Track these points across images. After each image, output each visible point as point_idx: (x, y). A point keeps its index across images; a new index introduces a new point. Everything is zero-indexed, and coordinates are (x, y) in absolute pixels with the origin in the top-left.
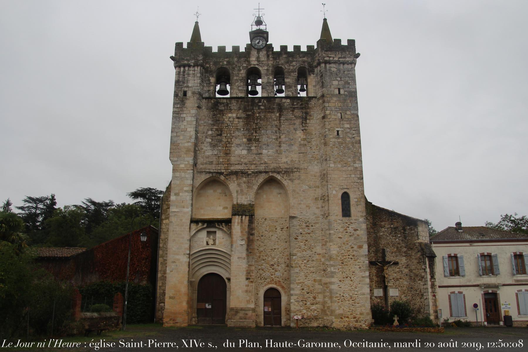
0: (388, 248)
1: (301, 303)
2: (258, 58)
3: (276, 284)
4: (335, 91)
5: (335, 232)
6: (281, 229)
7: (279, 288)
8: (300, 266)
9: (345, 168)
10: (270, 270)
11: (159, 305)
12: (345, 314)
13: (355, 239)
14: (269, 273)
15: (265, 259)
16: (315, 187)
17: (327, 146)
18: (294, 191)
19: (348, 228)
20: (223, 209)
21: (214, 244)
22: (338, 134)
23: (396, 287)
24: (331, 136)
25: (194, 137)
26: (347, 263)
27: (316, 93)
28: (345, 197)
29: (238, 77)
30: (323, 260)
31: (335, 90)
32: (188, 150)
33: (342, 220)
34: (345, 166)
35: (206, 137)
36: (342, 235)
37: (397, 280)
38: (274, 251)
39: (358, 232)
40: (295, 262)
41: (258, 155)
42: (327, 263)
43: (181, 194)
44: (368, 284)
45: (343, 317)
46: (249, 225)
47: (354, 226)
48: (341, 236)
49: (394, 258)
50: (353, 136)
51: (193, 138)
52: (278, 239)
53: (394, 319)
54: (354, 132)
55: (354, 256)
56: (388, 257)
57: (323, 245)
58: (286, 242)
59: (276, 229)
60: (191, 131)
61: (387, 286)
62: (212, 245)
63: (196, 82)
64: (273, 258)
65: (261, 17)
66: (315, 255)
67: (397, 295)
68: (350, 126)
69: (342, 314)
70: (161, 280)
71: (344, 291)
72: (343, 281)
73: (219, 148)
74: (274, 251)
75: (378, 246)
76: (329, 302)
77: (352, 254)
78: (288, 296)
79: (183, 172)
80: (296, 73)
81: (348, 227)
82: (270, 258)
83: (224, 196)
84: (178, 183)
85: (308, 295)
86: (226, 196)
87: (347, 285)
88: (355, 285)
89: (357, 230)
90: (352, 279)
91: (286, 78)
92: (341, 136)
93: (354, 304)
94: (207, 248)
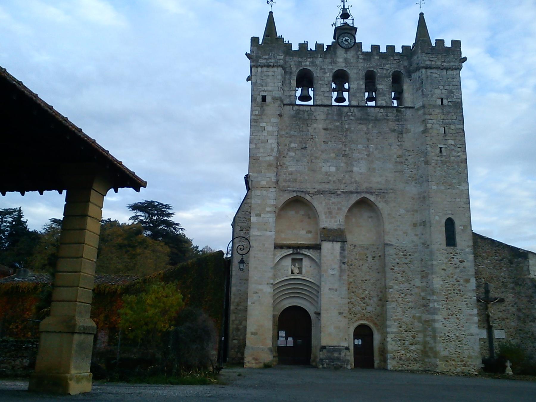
0: (492, 283)
1: (399, 343)
2: (346, 60)
3: (367, 320)
4: (437, 101)
5: (438, 263)
6: (372, 258)
7: (371, 325)
8: (396, 300)
9: (449, 190)
10: (360, 304)
11: (232, 341)
12: (450, 357)
13: (461, 271)
14: (359, 307)
15: (355, 291)
16: (413, 211)
17: (428, 165)
18: (389, 214)
19: (452, 259)
20: (307, 233)
21: (300, 273)
22: (441, 151)
23: (502, 328)
24: (433, 154)
25: (276, 150)
26: (452, 299)
27: (413, 102)
28: (450, 224)
29: (323, 81)
30: (423, 294)
31: (438, 99)
32: (270, 165)
33: (446, 250)
34: (449, 189)
35: (289, 150)
36: (446, 267)
37: (503, 320)
38: (365, 282)
39: (464, 264)
40: (391, 295)
41: (348, 173)
42: (428, 298)
43: (262, 215)
44: (476, 323)
45: (449, 361)
46: (341, 253)
47: (459, 257)
48: (445, 268)
49: (499, 295)
50: (458, 154)
51: (275, 151)
52: (370, 269)
53: (506, 364)
54: (459, 149)
55: (459, 290)
56: (492, 293)
57: (422, 277)
58: (379, 273)
59: (367, 257)
60: (272, 142)
61: (492, 326)
62: (297, 274)
63: (276, 85)
64: (365, 290)
65: (348, 10)
66: (414, 288)
67: (504, 337)
68: (454, 142)
69: (448, 356)
70: (234, 313)
71: (449, 330)
72: (448, 319)
73: (304, 163)
74: (365, 282)
75: (480, 281)
76: (432, 342)
77: (457, 288)
78: (382, 334)
79: (264, 190)
80: (391, 79)
81: (453, 258)
82: (361, 291)
83: (307, 218)
84: (260, 203)
85: (406, 333)
86: (309, 218)
87: (453, 323)
88: (461, 323)
89: (464, 261)
90: (458, 316)
91: (378, 84)
92: (444, 154)
93: (460, 346)
94: (292, 277)
